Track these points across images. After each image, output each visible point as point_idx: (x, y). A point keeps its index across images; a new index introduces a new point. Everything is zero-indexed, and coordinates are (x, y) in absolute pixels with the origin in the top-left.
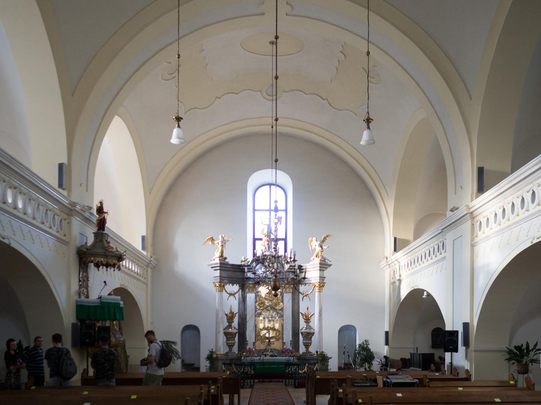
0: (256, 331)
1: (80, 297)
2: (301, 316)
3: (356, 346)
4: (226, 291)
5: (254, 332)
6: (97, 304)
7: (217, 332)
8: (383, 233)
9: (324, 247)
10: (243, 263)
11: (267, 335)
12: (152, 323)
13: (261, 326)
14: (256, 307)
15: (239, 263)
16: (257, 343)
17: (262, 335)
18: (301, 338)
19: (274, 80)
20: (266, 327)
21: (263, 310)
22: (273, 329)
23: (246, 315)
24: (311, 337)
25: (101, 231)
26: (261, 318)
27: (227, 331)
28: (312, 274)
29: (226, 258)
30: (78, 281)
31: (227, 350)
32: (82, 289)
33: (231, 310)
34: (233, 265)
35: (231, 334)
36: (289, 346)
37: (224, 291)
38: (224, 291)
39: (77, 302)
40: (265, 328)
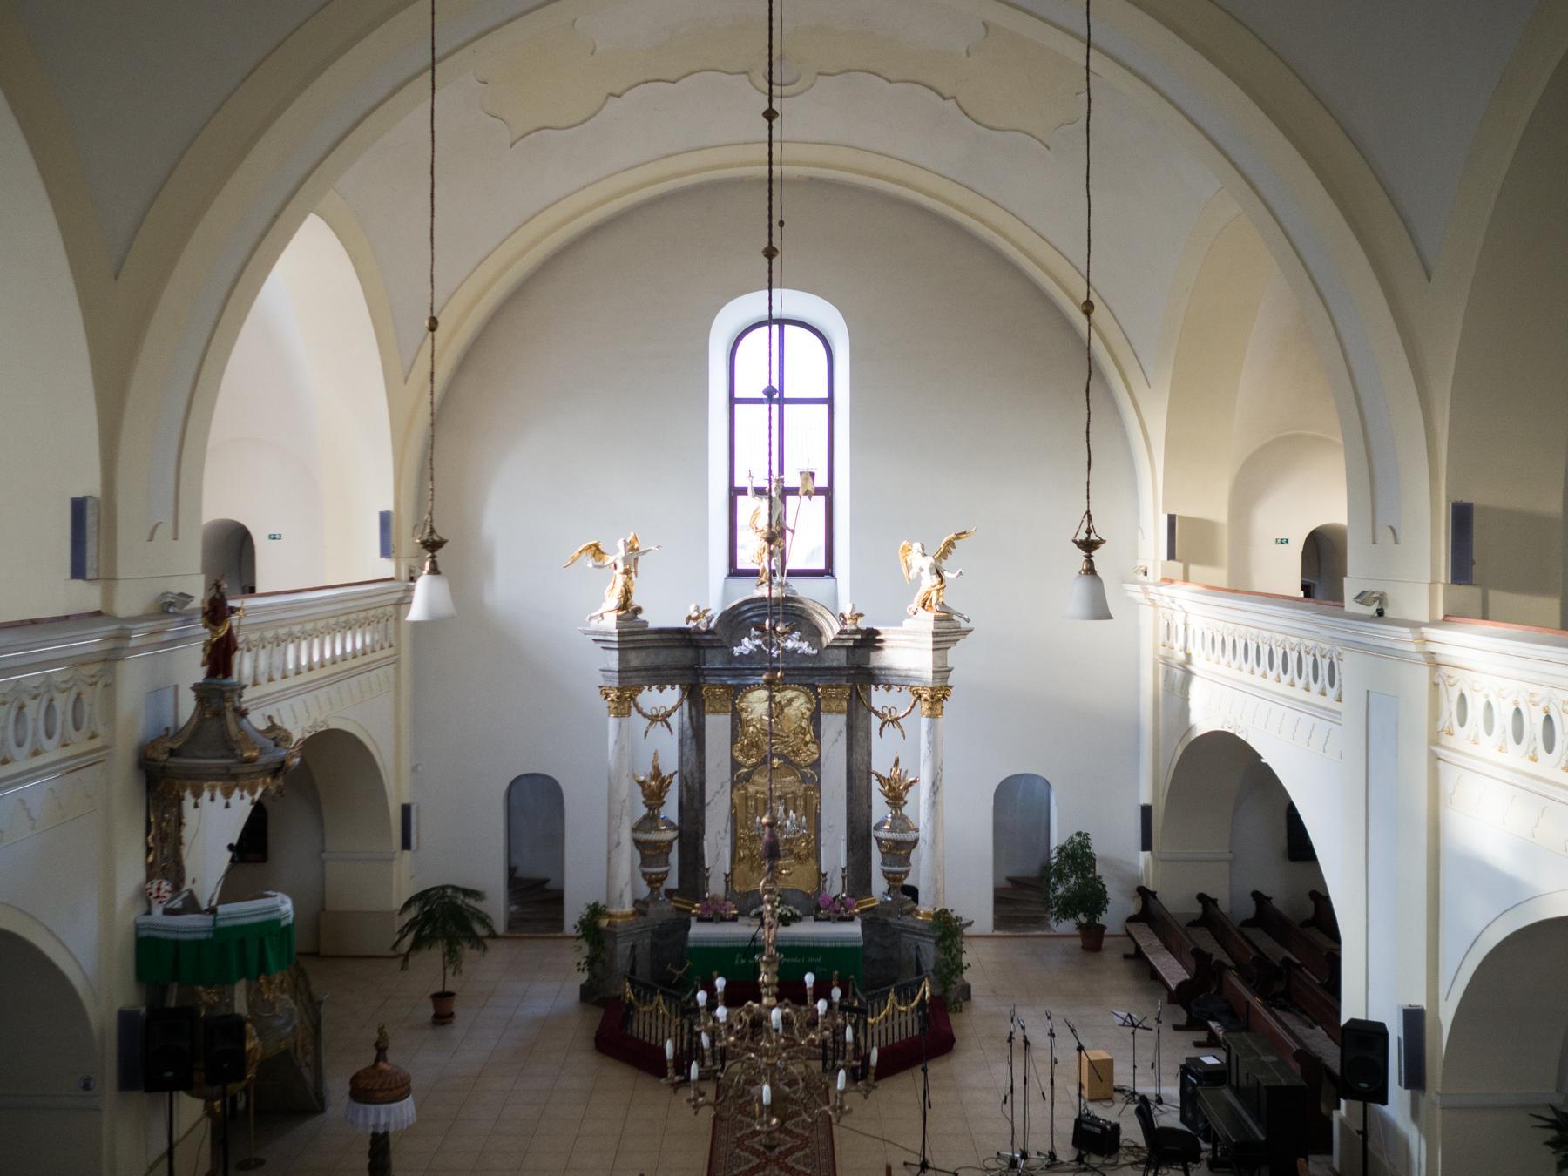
1: (149, 913)
2: (876, 785)
3: (1049, 853)
4: (640, 711)
6: (202, 936)
7: (613, 846)
8: (1136, 511)
9: (946, 575)
10: (692, 624)
12: (414, 769)
14: (733, 758)
15: (683, 625)
18: (876, 855)
19: (776, 244)
21: (754, 766)
23: (702, 785)
24: (909, 854)
25: (219, 680)
27: (643, 836)
28: (907, 651)
29: (638, 610)
30: (142, 851)
32: (156, 882)
33: (656, 768)
35: (655, 845)
36: (835, 887)
37: (633, 710)
38: (633, 710)
39: (138, 928)
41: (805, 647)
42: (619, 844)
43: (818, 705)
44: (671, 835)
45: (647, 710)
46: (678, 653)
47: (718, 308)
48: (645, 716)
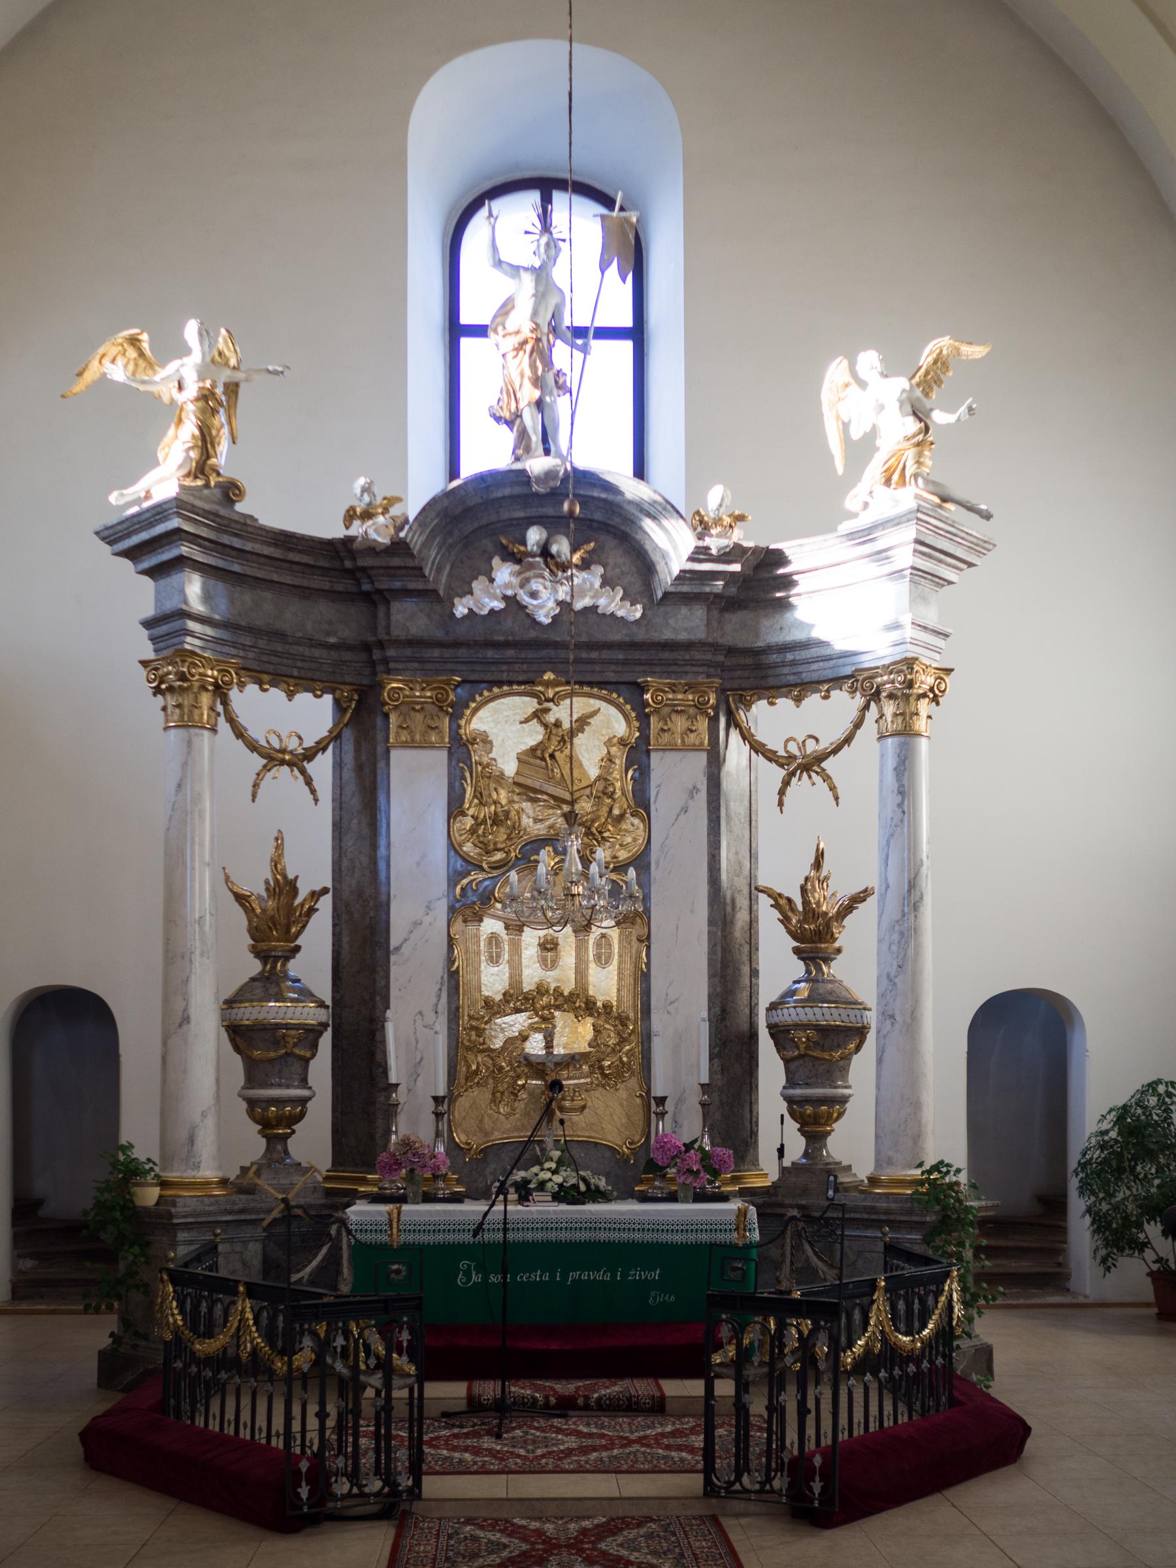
0: (454, 1014)
4: (239, 732)
5: (442, 1024)
9: (939, 417)
11: (535, 1046)
13: (493, 980)
15: (333, 530)
16: (463, 1103)
17: (498, 1044)
20: (528, 985)
22: (580, 1003)
24: (847, 1058)
26: (491, 926)
27: (248, 1014)
31: (252, 1144)
34: (285, 540)
35: (271, 1033)
36: (687, 1125)
40: (517, 999)
41: (613, 603)
42: (186, 1020)
43: (644, 728)
44: (310, 1014)
45: (257, 733)
46: (324, 610)
47: (428, 73)
48: (253, 746)
